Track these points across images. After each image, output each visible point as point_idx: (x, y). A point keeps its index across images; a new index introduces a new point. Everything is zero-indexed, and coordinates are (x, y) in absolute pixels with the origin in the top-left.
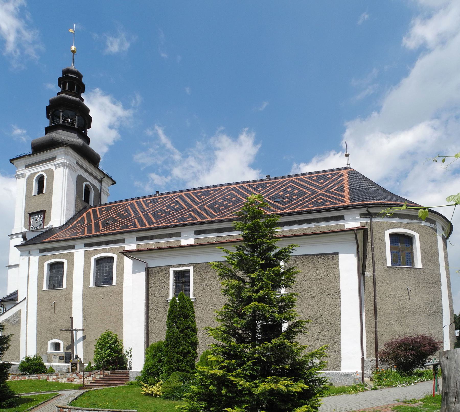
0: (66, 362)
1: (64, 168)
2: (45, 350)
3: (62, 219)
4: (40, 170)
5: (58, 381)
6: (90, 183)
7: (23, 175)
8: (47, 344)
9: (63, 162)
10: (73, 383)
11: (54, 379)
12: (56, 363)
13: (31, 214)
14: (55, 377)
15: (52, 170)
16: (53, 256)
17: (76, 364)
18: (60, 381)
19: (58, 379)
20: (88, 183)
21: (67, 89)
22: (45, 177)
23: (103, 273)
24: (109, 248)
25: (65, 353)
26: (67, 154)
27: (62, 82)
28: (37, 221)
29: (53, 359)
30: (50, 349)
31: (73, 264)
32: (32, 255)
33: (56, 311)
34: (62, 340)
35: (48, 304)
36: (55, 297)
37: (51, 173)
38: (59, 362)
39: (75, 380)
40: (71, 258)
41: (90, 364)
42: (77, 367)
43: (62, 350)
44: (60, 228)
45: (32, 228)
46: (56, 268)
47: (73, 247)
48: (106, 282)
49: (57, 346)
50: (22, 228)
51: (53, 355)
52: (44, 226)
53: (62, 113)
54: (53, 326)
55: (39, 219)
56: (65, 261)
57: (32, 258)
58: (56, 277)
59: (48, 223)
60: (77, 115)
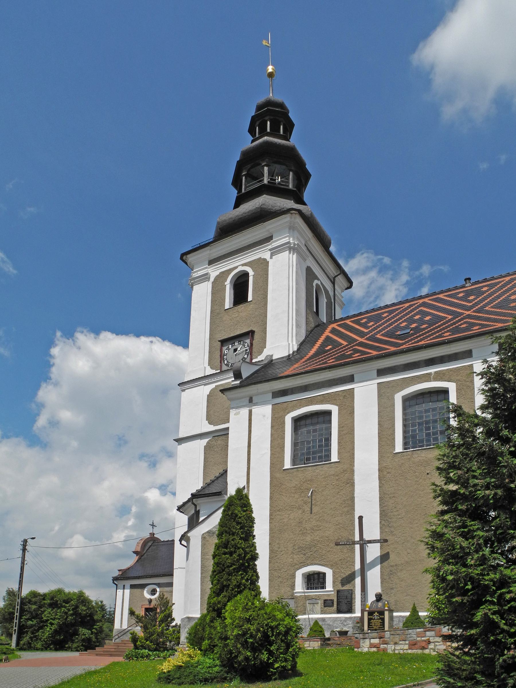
0: (339, 611)
1: (290, 253)
2: (289, 589)
3: (290, 342)
4: (238, 264)
5: (385, 650)
6: (321, 283)
7: (205, 277)
8: (294, 576)
9: (289, 243)
10: (427, 651)
11: (372, 646)
12: (314, 613)
13: (224, 342)
14: (376, 641)
15: (265, 260)
16: (303, 402)
17: (381, 613)
18: (390, 648)
19: (382, 646)
20: (319, 283)
21: (268, 130)
22: (251, 273)
23: (420, 424)
24: (436, 372)
25: (338, 592)
26: (292, 228)
27: (258, 123)
28: (235, 354)
29: (309, 607)
30: (299, 587)
31: (352, 413)
32: (256, 404)
33: (315, 509)
34: (331, 567)
35: (297, 496)
36: (311, 480)
37: (262, 266)
38: (322, 612)
39: (431, 646)
40: (347, 402)
41: (415, 611)
42: (383, 619)
43: (329, 586)
44: (289, 359)
45: (227, 365)
46: (313, 423)
47: (351, 379)
48: (428, 440)
49: (315, 580)
50: (205, 368)
51: (307, 598)
52: (251, 359)
53: (266, 168)
54: (308, 538)
55: (241, 347)
56: (335, 410)
57: (256, 410)
58: (308, 443)
59: (260, 353)
60: (291, 170)
